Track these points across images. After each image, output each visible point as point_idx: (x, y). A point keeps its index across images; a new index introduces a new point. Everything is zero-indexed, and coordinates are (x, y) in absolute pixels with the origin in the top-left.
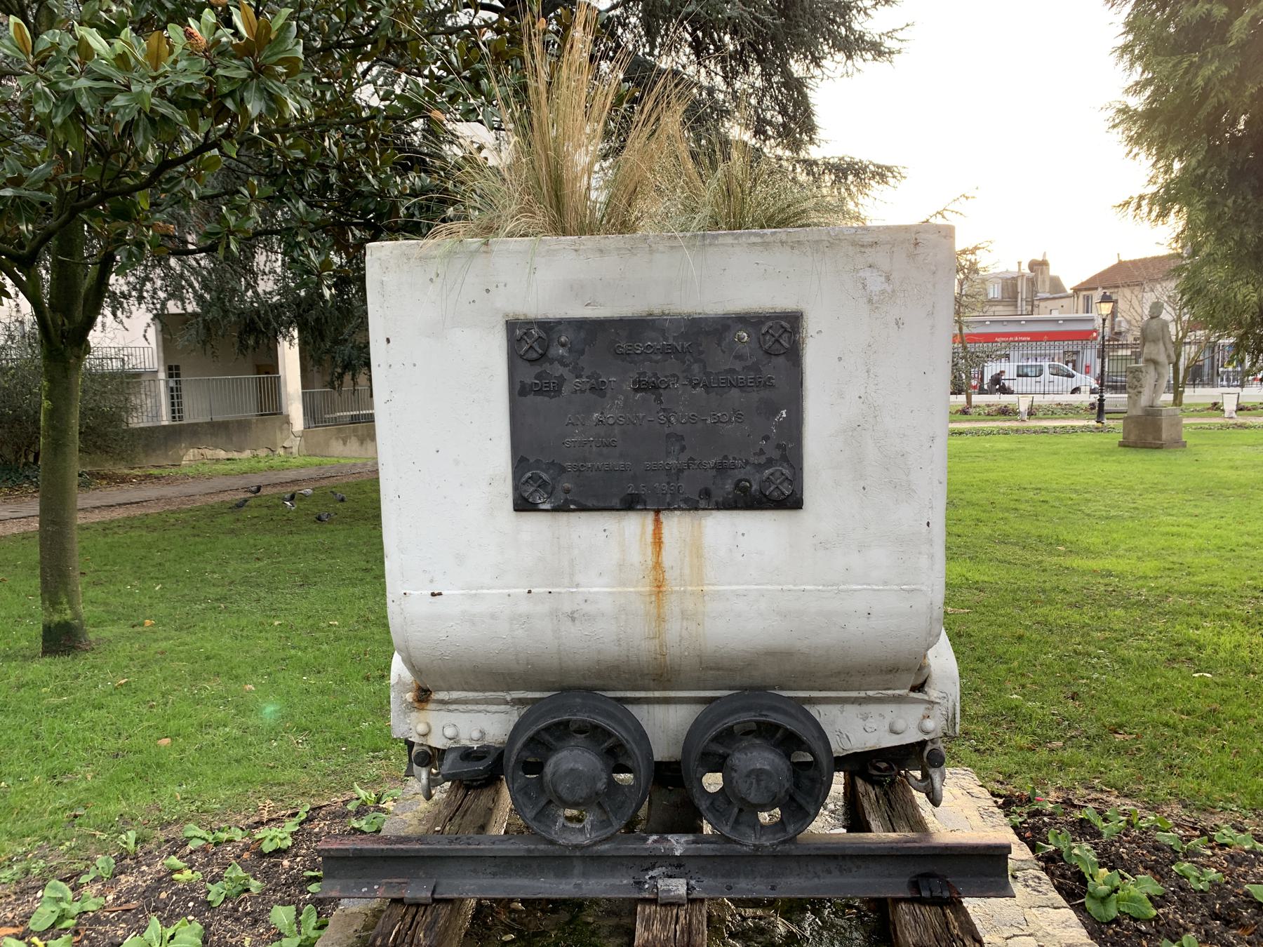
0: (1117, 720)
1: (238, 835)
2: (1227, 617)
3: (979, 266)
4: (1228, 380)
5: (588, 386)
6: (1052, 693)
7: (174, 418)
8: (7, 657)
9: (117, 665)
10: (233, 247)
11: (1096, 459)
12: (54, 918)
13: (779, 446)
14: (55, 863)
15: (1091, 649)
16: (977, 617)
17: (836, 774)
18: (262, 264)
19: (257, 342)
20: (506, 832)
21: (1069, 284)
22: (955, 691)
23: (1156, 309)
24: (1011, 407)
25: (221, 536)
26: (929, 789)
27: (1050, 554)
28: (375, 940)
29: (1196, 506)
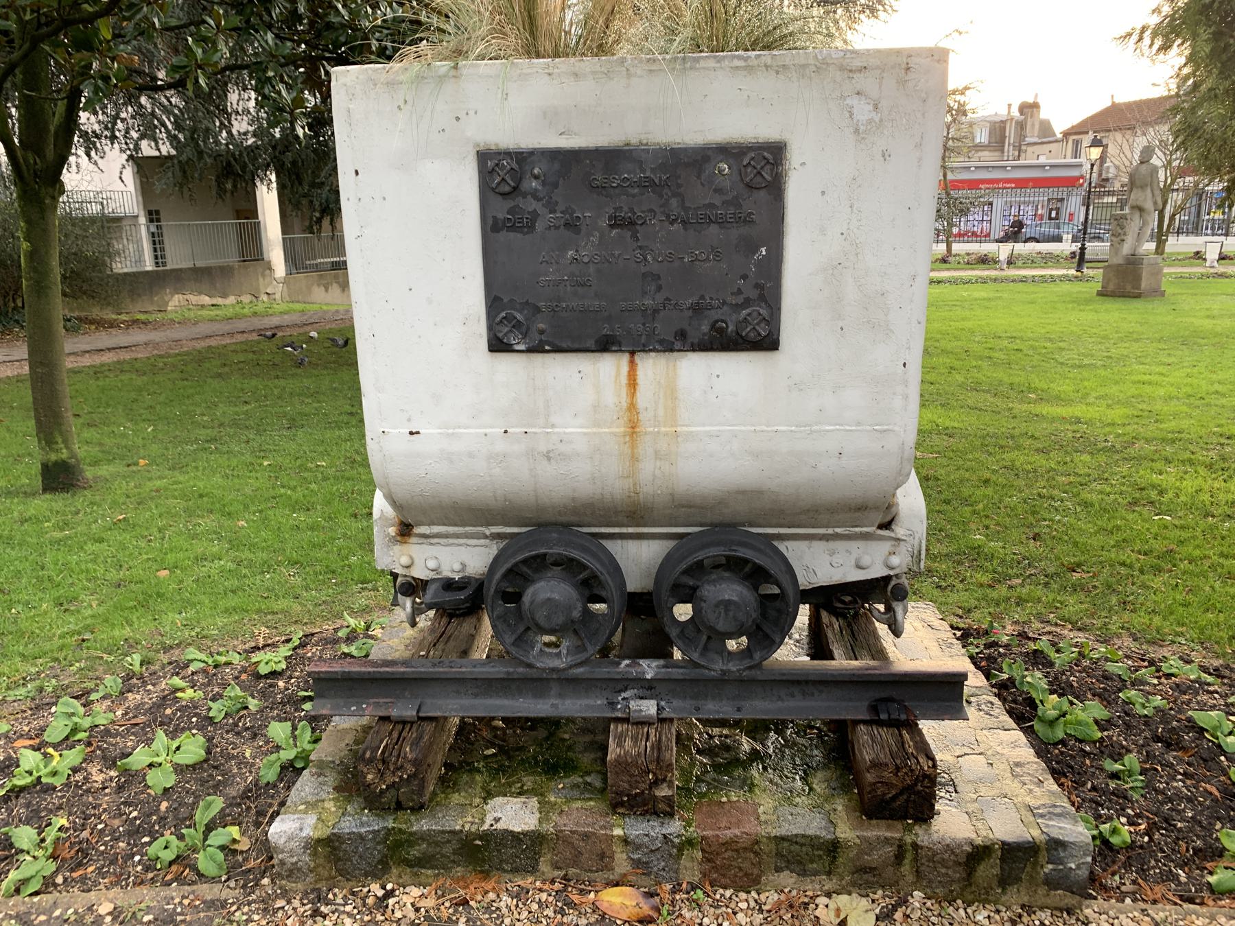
0: (1076, 559)
1: (236, 659)
2: (1191, 463)
3: (967, 108)
4: (1213, 229)
5: (562, 222)
6: (1015, 534)
7: (157, 263)
8: (9, 494)
9: (114, 502)
10: (202, 82)
11: (1073, 309)
12: (68, 730)
13: (757, 286)
14: (66, 682)
15: (1056, 492)
16: (945, 461)
17: (801, 606)
18: (235, 103)
19: (235, 186)
20: (488, 657)
21: (1059, 128)
22: (921, 528)
23: (1147, 153)
24: (991, 255)
25: (209, 380)
26: (891, 621)
27: (1021, 401)
28: (364, 753)
29: (1169, 354)
